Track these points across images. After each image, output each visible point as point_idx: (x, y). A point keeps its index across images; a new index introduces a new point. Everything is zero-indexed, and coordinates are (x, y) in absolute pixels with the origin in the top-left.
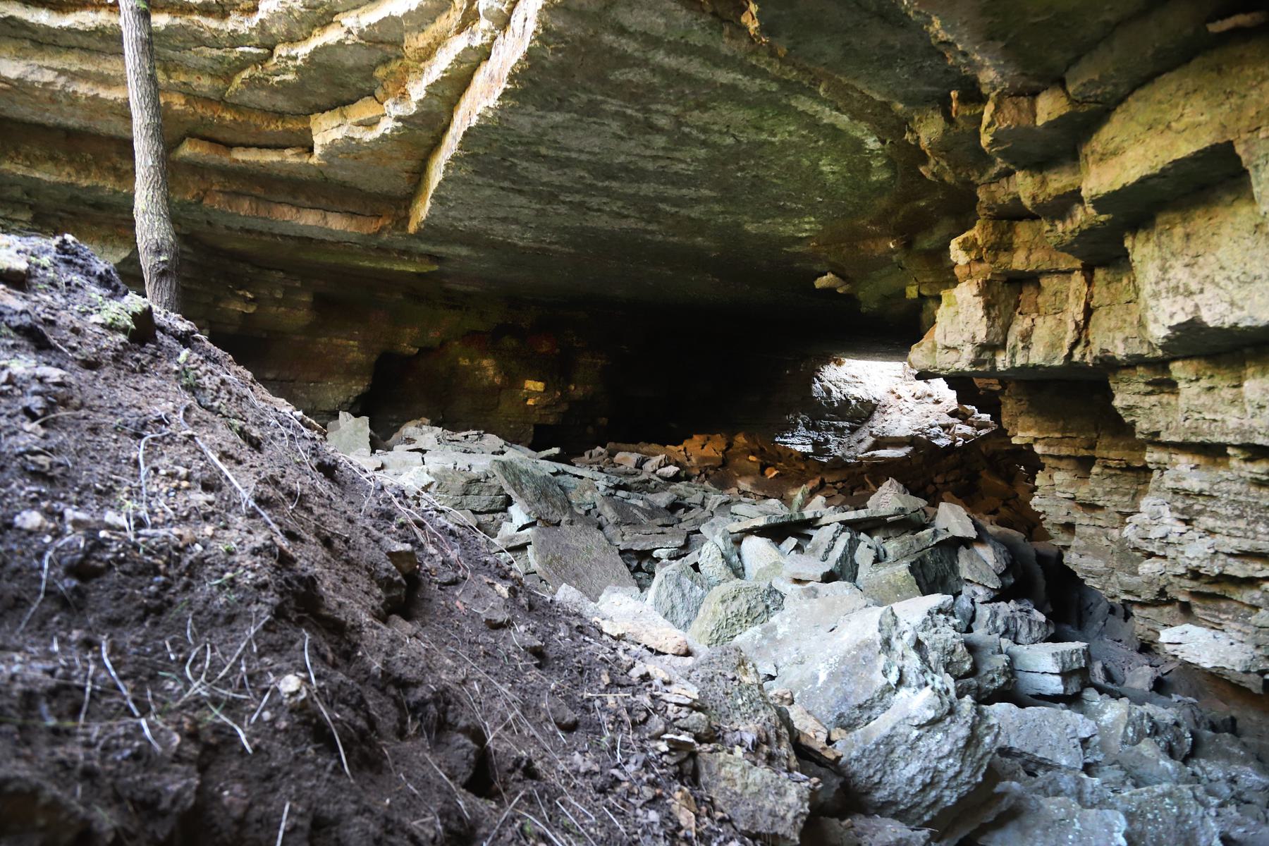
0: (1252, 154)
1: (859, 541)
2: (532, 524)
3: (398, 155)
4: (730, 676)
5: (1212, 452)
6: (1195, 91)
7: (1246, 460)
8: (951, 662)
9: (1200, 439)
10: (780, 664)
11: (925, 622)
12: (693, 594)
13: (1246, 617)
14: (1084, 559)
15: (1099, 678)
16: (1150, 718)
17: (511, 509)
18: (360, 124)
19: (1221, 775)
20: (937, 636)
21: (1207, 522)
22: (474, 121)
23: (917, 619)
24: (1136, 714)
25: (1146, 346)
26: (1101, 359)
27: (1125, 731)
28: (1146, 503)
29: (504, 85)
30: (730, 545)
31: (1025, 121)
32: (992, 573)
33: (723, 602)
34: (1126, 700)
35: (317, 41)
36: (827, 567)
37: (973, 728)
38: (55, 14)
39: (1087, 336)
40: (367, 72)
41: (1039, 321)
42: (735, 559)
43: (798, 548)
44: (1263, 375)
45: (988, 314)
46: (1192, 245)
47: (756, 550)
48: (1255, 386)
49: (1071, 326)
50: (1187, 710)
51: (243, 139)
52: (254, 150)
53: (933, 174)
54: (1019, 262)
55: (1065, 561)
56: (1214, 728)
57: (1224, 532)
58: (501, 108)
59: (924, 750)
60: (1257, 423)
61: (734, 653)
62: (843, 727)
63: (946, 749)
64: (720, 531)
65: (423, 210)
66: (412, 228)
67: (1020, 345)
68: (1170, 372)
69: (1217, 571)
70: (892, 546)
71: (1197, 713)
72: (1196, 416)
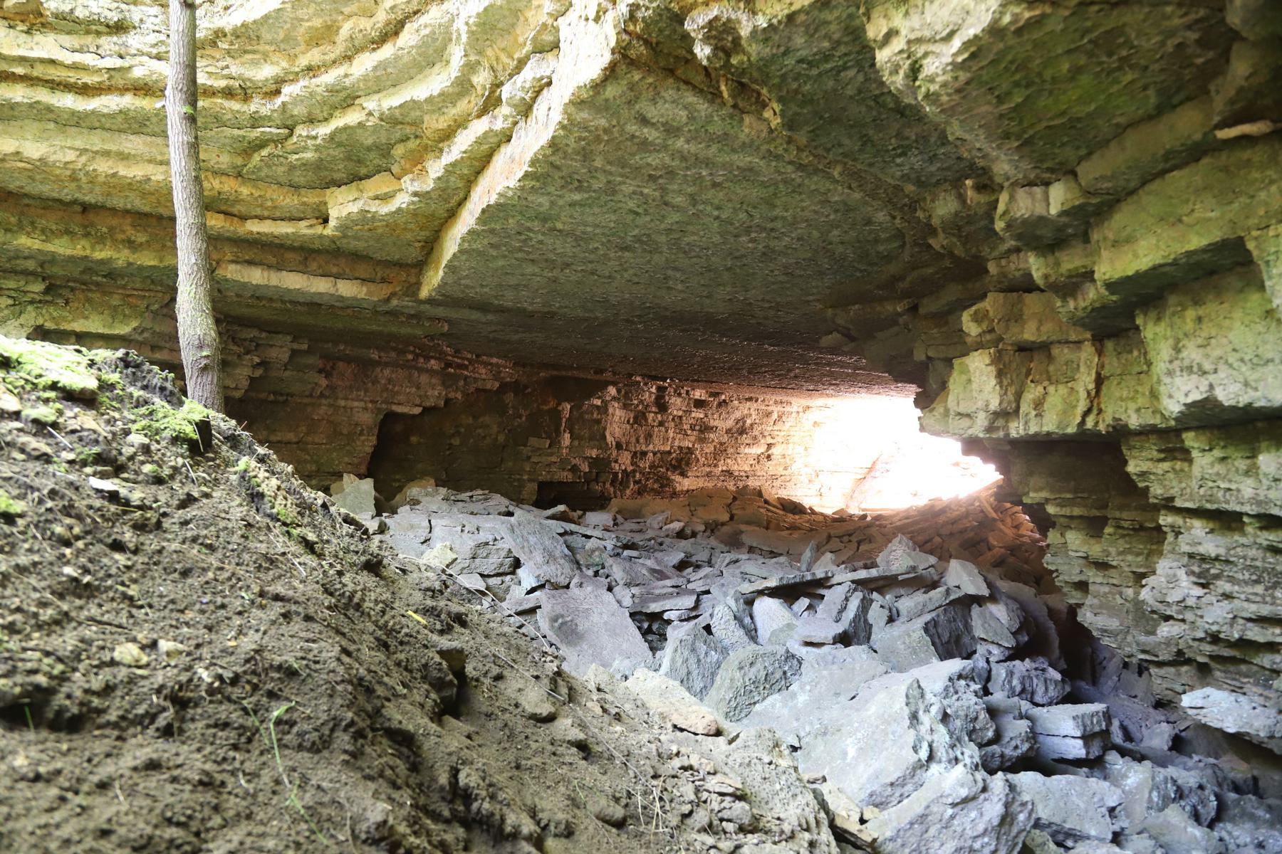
0: (1262, 251)
1: (872, 601)
2: (542, 587)
3: (412, 226)
4: (767, 760)
5: (1226, 520)
6: (1205, 188)
7: (1261, 528)
8: (974, 730)
9: (1214, 507)
10: (802, 734)
11: (946, 689)
12: (709, 660)
13: (1267, 680)
14: (1099, 618)
15: (1118, 737)
16: (1174, 781)
17: (519, 571)
18: (376, 198)
19: (1248, 840)
20: (957, 704)
21: (1223, 586)
22: (493, 199)
23: (939, 686)
24: (1159, 778)
25: (1158, 416)
26: (1114, 427)
27: (1150, 797)
28: (1164, 566)
29: (526, 168)
30: (742, 606)
31: (1040, 210)
32: (1006, 631)
33: (741, 668)
34: (1147, 763)
35: (338, 122)
36: (839, 628)
37: (1007, 805)
38: (80, 98)
39: (1099, 404)
40: (385, 151)
41: (1051, 389)
42: (747, 620)
43: (810, 607)
44: (1278, 450)
45: (1000, 383)
46: (1204, 327)
47: (769, 611)
48: (1268, 461)
49: (1083, 395)
50: (1209, 771)
51: (258, 211)
52: (268, 222)
53: (943, 246)
54: (1029, 333)
55: (1079, 619)
56: (1237, 788)
57: (1243, 596)
58: (522, 189)
59: (959, 829)
60: (1272, 494)
61: (768, 735)
62: (876, 806)
63: (981, 828)
64: (732, 592)
65: (433, 279)
66: (424, 293)
67: (1034, 413)
68: (1183, 441)
69: (1236, 636)
70: (907, 603)
71: (1219, 773)
72: (1211, 484)
